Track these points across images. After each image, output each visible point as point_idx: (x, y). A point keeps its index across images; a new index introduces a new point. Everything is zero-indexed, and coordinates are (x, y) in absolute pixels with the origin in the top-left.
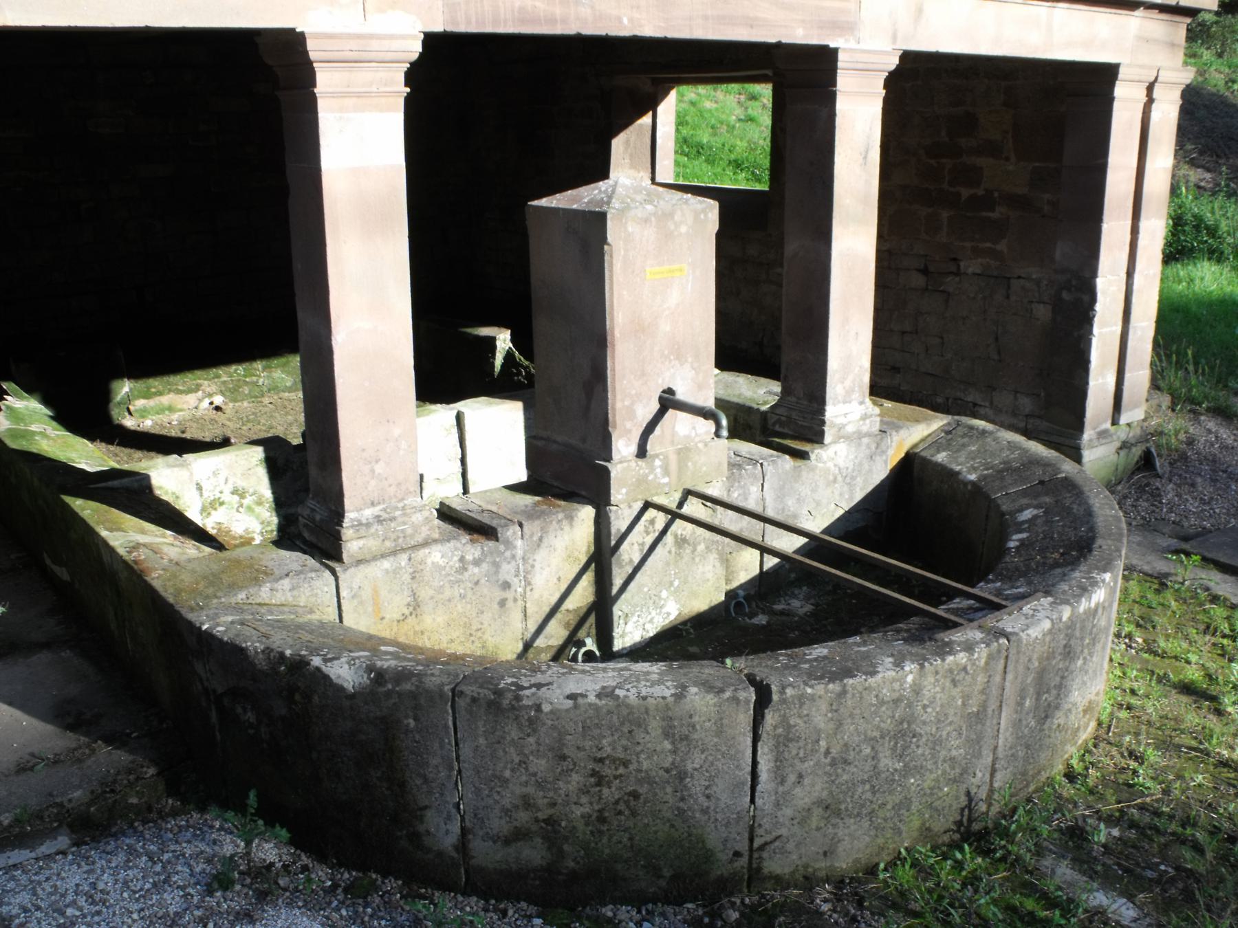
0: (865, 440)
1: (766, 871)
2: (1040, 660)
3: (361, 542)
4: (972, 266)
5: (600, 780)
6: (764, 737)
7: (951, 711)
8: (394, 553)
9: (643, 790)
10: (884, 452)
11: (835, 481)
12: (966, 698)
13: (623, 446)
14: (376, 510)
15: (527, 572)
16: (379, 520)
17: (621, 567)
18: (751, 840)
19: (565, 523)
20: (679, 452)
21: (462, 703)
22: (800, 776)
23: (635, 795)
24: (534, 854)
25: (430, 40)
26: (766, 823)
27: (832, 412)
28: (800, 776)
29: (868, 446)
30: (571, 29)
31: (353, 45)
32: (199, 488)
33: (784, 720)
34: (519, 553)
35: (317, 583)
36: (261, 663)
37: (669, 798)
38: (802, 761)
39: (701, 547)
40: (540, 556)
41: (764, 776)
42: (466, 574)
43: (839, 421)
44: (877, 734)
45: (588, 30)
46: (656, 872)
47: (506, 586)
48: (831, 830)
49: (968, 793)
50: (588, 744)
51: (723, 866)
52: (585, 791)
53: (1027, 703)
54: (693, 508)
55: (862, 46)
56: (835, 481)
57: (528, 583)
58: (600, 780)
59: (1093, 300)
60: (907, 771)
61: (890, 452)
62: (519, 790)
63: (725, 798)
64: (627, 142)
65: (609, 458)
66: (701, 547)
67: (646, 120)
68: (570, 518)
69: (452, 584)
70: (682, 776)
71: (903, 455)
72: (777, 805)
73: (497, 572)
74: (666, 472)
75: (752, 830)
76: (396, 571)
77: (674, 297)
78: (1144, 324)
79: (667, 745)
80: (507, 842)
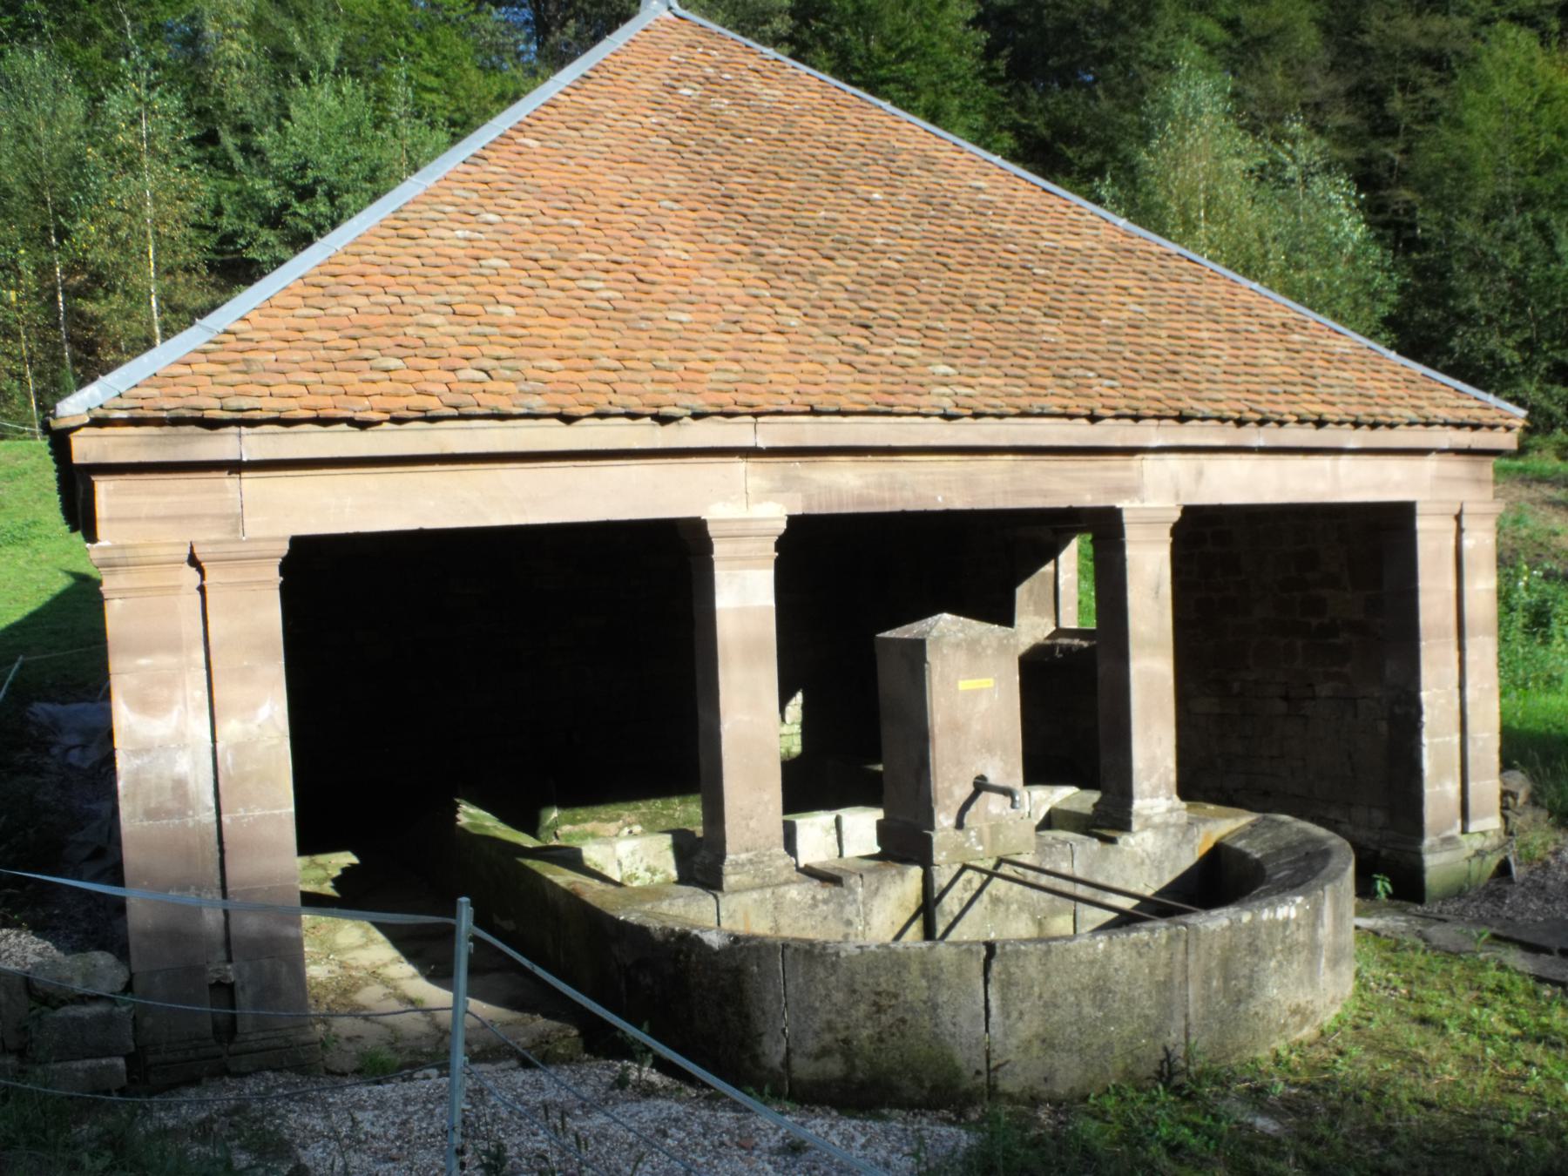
0: (1172, 830)
1: (1000, 1089)
2: (1222, 949)
3: (737, 877)
4: (1324, 690)
5: (879, 1009)
6: (992, 981)
7: (1141, 977)
8: (762, 887)
9: (908, 1017)
10: (1190, 841)
11: (1143, 863)
12: (1153, 968)
13: (944, 820)
14: (750, 855)
15: (866, 915)
16: (751, 861)
17: (943, 915)
18: (988, 1062)
19: (898, 878)
20: (991, 827)
21: (788, 952)
22: (1021, 1014)
23: (903, 1021)
24: (834, 1067)
25: (792, 520)
26: (998, 1048)
27: (1138, 805)
28: (1021, 1014)
29: (1175, 835)
30: (897, 507)
31: (738, 526)
32: (620, 864)
33: (1006, 969)
34: (860, 898)
35: (704, 903)
36: (659, 937)
37: (926, 1024)
38: (1022, 1001)
39: (1014, 907)
40: (877, 903)
41: (994, 1011)
42: (817, 911)
43: (1146, 812)
44: (1078, 986)
45: (911, 507)
46: (919, 1081)
47: (849, 923)
48: (1048, 1060)
49: (1165, 1049)
50: (871, 981)
51: (968, 1082)
52: (869, 1017)
53: (1215, 983)
54: (1006, 869)
55: (1147, 505)
56: (1143, 863)
57: (867, 923)
58: (879, 1009)
59: (1419, 712)
60: (1107, 1020)
61: (1198, 841)
62: (825, 1017)
63: (966, 1026)
64: (1031, 591)
65: (932, 828)
66: (1014, 907)
67: (1049, 568)
68: (902, 874)
69: (806, 916)
70: (935, 1007)
71: (1210, 845)
72: (1006, 1035)
73: (841, 911)
74: (980, 841)
75: (988, 1053)
76: (763, 901)
77: (983, 705)
78: (1486, 735)
79: (924, 983)
80: (817, 1057)
